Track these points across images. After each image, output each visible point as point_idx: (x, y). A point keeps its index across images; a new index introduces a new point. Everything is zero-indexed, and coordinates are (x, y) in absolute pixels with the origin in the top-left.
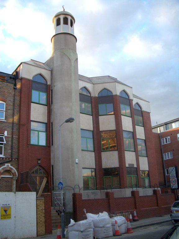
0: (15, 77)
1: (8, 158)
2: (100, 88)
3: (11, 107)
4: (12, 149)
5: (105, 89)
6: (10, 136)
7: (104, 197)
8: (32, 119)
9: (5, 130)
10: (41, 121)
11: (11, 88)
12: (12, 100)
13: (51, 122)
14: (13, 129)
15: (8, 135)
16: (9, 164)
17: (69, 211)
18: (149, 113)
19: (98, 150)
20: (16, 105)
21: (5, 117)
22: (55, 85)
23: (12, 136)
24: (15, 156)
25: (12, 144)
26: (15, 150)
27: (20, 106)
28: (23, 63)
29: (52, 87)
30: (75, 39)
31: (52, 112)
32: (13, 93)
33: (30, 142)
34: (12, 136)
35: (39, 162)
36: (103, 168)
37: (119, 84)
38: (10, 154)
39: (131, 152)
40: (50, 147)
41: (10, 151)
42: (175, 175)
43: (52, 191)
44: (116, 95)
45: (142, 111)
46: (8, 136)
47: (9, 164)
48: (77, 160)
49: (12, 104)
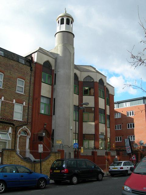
0: (29, 60)
1: (25, 122)
2: (85, 74)
3: (28, 85)
4: (28, 115)
5: (89, 76)
6: (27, 106)
7: (90, 154)
8: (42, 94)
9: (24, 101)
10: (47, 97)
11: (28, 69)
12: (29, 79)
13: (54, 98)
14: (29, 101)
15: (4, 100)
16: (26, 127)
17: (27, 157)
18: (113, 96)
19: (80, 121)
20: (31, 83)
21: (24, 91)
22: (58, 70)
23: (29, 106)
24: (30, 121)
25: (28, 112)
26: (30, 117)
27: (34, 84)
28: (121, 77)
29: (55, 72)
30: (72, 35)
31: (55, 91)
32: (30, 74)
33: (39, 111)
34: (29, 106)
35: (45, 126)
36: (83, 133)
37: (99, 74)
38: (27, 119)
39: (102, 124)
40: (52, 116)
41: (26, 117)
42: (129, 144)
43: (52, 148)
44: (97, 82)
45: (109, 94)
46: (26, 106)
47: (26, 127)
48: (71, 127)
49: (29, 82)
